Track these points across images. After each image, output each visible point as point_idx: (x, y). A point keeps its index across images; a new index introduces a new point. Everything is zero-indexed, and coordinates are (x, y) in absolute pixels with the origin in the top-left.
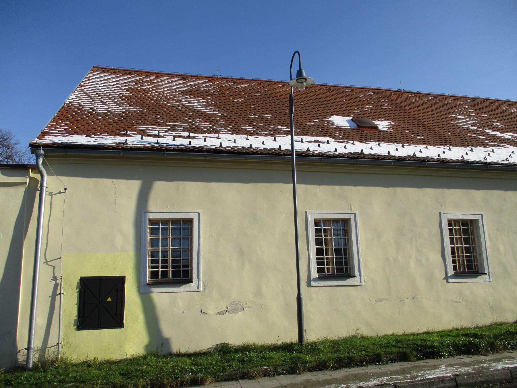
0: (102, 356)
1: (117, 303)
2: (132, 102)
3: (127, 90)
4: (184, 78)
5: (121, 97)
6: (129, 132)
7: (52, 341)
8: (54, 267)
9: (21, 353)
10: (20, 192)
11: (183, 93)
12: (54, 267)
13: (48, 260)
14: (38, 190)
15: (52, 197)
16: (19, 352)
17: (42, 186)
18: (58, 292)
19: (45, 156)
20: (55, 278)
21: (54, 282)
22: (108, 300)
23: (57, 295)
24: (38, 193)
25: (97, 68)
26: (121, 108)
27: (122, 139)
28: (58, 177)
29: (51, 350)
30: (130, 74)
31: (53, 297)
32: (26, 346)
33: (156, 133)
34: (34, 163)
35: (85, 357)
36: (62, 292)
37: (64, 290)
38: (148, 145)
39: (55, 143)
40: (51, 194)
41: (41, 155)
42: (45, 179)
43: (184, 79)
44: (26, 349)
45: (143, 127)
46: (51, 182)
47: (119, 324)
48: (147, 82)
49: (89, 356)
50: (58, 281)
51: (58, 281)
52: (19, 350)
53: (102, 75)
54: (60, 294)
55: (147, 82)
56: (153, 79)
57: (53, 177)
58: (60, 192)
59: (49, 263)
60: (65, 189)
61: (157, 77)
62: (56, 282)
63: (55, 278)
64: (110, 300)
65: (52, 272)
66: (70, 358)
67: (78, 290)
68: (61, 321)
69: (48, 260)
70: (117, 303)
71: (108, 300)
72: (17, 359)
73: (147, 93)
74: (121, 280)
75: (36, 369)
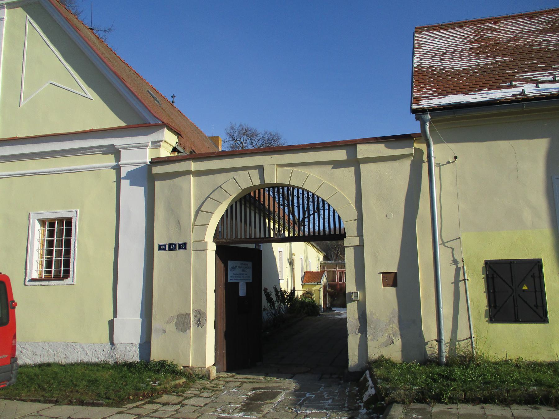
0: (528, 356)
1: (535, 292)
2: (487, 53)
3: (472, 43)
4: (531, 16)
5: (469, 51)
6: (514, 83)
7: (463, 333)
8: (453, 249)
9: (429, 345)
10: (406, 165)
11: (544, 31)
12: (453, 249)
13: (445, 241)
14: (424, 162)
15: (440, 169)
16: (427, 343)
17: (429, 157)
18: (461, 278)
19: (432, 122)
20: (455, 262)
21: (454, 267)
22: (524, 288)
23: (461, 281)
24: (425, 166)
25: (420, 28)
26: (479, 61)
27: (517, 91)
28: (449, 145)
29: (462, 344)
30: (461, 26)
31: (456, 282)
32: (436, 337)
33: (551, 78)
34: (418, 130)
35: (504, 355)
36: (466, 278)
37: (468, 275)
38: (554, 92)
39: (439, 106)
40: (439, 165)
41: (427, 120)
42: (432, 148)
43: (531, 18)
44: (437, 341)
45: (527, 75)
46: (439, 152)
47: (541, 318)
48: (488, 30)
49: (508, 354)
50: (459, 266)
51: (460, 265)
52: (426, 341)
53: (431, 34)
54: (464, 280)
55: (488, 30)
56: (491, 25)
57: (444, 144)
58: (449, 162)
59: (446, 244)
60: (456, 158)
61: (495, 23)
62: (457, 266)
63: (455, 262)
64: (526, 288)
65: (451, 254)
66: (485, 355)
67: (484, 276)
68: (470, 309)
69: (445, 241)
70: (535, 292)
71: (524, 288)
72: (426, 352)
73: (497, 40)
74: (538, 264)
75: (447, 364)
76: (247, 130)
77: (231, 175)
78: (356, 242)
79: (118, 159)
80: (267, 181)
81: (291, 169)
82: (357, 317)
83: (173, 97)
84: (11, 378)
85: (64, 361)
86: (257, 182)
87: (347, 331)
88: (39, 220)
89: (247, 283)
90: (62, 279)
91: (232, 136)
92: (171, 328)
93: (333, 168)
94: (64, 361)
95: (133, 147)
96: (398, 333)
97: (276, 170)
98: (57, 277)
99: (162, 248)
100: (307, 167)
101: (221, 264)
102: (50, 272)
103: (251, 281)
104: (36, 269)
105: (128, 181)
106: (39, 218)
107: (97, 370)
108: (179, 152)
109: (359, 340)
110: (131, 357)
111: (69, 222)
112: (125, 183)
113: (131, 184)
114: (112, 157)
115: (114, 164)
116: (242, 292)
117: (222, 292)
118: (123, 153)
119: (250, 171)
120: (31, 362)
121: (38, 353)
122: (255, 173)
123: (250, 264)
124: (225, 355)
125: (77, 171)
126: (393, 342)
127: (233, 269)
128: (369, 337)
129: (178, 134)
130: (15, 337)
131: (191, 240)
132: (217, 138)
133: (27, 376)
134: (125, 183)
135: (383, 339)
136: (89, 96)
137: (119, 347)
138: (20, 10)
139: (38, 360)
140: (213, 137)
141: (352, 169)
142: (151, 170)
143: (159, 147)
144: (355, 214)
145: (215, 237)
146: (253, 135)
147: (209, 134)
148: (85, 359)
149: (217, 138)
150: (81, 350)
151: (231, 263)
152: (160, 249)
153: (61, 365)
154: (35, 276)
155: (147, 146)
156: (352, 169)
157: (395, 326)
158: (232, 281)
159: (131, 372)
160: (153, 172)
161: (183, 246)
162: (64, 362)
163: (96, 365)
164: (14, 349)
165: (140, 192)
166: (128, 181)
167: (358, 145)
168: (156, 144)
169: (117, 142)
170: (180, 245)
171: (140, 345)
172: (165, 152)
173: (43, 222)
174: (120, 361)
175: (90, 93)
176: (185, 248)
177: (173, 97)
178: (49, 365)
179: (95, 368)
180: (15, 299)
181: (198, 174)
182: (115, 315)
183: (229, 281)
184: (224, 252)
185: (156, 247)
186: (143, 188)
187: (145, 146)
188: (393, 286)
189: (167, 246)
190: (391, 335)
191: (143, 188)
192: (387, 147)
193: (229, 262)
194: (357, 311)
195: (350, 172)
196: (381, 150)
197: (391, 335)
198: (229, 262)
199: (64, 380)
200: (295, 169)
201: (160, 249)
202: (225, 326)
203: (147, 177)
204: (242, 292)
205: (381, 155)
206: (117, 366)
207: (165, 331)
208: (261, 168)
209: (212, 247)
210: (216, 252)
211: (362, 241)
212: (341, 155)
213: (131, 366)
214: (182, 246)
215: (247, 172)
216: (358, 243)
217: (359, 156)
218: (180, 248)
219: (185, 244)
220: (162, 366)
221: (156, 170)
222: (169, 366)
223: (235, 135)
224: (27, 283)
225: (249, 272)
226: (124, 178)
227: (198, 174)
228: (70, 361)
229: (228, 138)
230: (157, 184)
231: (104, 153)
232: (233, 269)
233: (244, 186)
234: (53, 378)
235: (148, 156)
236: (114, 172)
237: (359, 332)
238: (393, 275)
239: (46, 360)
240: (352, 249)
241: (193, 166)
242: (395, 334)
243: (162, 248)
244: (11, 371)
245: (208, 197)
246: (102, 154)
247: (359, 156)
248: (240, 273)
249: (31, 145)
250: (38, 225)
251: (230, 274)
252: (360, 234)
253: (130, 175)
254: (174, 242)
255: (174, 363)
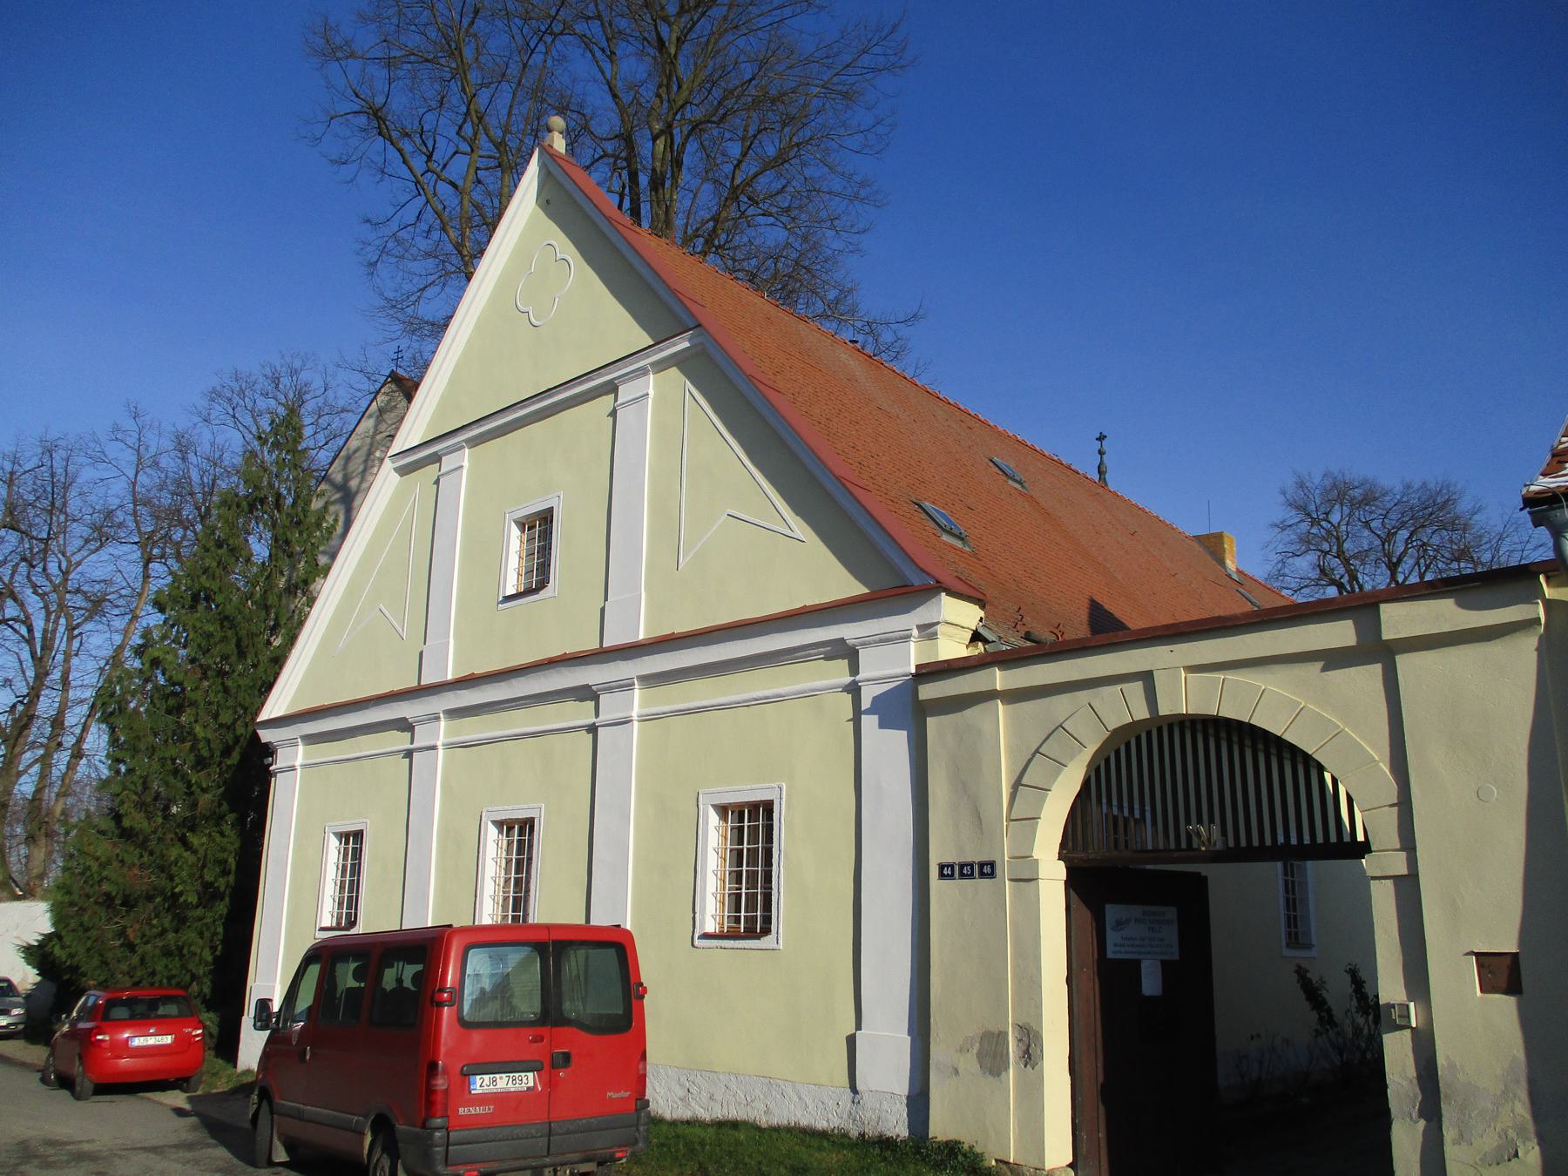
76: (1349, 486)
77: (1083, 696)
78: (1398, 864)
79: (854, 669)
80: (1164, 709)
81: (1221, 676)
82: (1412, 1072)
83: (1101, 438)
84: (636, 1142)
85: (764, 1120)
86: (1142, 713)
87: (1388, 1111)
88: (714, 806)
89: (1163, 963)
90: (758, 938)
91: (1302, 508)
92: (969, 1063)
93: (1324, 669)
94: (764, 1120)
95: (881, 641)
96: (1531, 1127)
97: (1187, 682)
98: (751, 933)
99: (946, 871)
100: (1260, 669)
101: (1085, 914)
102: (738, 920)
103: (1176, 957)
104: (712, 916)
105: (875, 718)
106: (717, 802)
107: (820, 1149)
108: (986, 641)
109: (1420, 1139)
110: (891, 1125)
111: (768, 807)
112: (869, 722)
113: (882, 726)
114: (843, 664)
115: (849, 679)
116: (1151, 985)
117: (1091, 987)
118: (863, 654)
119: (1125, 686)
120: (705, 1116)
121: (718, 1097)
122: (1136, 689)
123: (1171, 913)
124: (1103, 1144)
125: (779, 699)
126: (1516, 1155)
127: (1119, 924)
128: (1449, 1134)
129: (981, 603)
130: (644, 1057)
131: (1005, 857)
132: (1218, 537)
133: (686, 1145)
134: (869, 722)
135: (1488, 1141)
136: (799, 534)
137: (867, 1099)
138: (674, 372)
139: (718, 1113)
140: (1208, 536)
141: (1377, 668)
142: (916, 692)
143: (933, 637)
144: (1391, 791)
145: (1063, 846)
146: (1368, 499)
147: (1193, 526)
148: (804, 1122)
149: (1218, 537)
150: (795, 1098)
151: (1112, 912)
152: (942, 876)
153: (759, 1129)
154: (711, 927)
155: (909, 636)
156: (1377, 668)
157: (1521, 1109)
158: (1119, 956)
159: (885, 1159)
160: (922, 697)
161: (987, 870)
162: (764, 1121)
163: (823, 1135)
164: (642, 1080)
165: (898, 740)
166: (875, 718)
167: (1383, 607)
168: (928, 631)
169: (849, 632)
170: (982, 865)
171: (908, 1097)
172: (953, 647)
173: (722, 810)
174: (871, 1132)
175: (800, 528)
176: (992, 875)
177: (1101, 438)
178: (735, 1125)
179: (815, 1142)
180: (645, 977)
181: (1014, 696)
182: (859, 1027)
183: (1110, 955)
184: (1089, 883)
185: (934, 872)
186: (905, 733)
187: (906, 638)
188: (1507, 992)
189: (976, 868)
190: (1512, 1134)
191: (905, 733)
192: (1462, 605)
193: (1108, 907)
194: (1411, 1055)
195: (1369, 677)
196: (1444, 614)
197: (1512, 1134)
198: (1108, 907)
199: (747, 1159)
200: (1231, 676)
201: (942, 876)
202: (1100, 1071)
203: (911, 706)
204: (1151, 985)
205: (1446, 628)
206: (863, 1142)
207: (956, 1071)
208: (1147, 677)
209: (1052, 875)
210: (1069, 884)
211: (1412, 862)
212: (1341, 633)
213: (886, 1144)
214: (987, 870)
215: (1119, 687)
216: (1402, 870)
217: (1387, 634)
218: (982, 875)
219: (992, 864)
220: (949, 1155)
221: (928, 691)
222: (964, 1155)
223: (1313, 507)
224: (697, 942)
225: (1170, 935)
226: (868, 712)
227: (1014, 696)
228: (775, 1121)
229: (1293, 516)
230: (931, 722)
231: (828, 658)
232: (1119, 924)
233: (1114, 723)
234: (730, 1154)
235: (913, 656)
236: (847, 698)
237: (1422, 1114)
238: (1507, 961)
239: (734, 1113)
240: (1389, 883)
241: (1000, 679)
242: (1521, 1130)
243: (946, 871)
244: (637, 1126)
245: (1037, 751)
246: (826, 659)
247: (1387, 634)
248: (1146, 941)
249: (695, 651)
250: (714, 818)
251: (1112, 938)
252: (1408, 843)
253: (879, 704)
254: (969, 860)
255: (978, 1150)
